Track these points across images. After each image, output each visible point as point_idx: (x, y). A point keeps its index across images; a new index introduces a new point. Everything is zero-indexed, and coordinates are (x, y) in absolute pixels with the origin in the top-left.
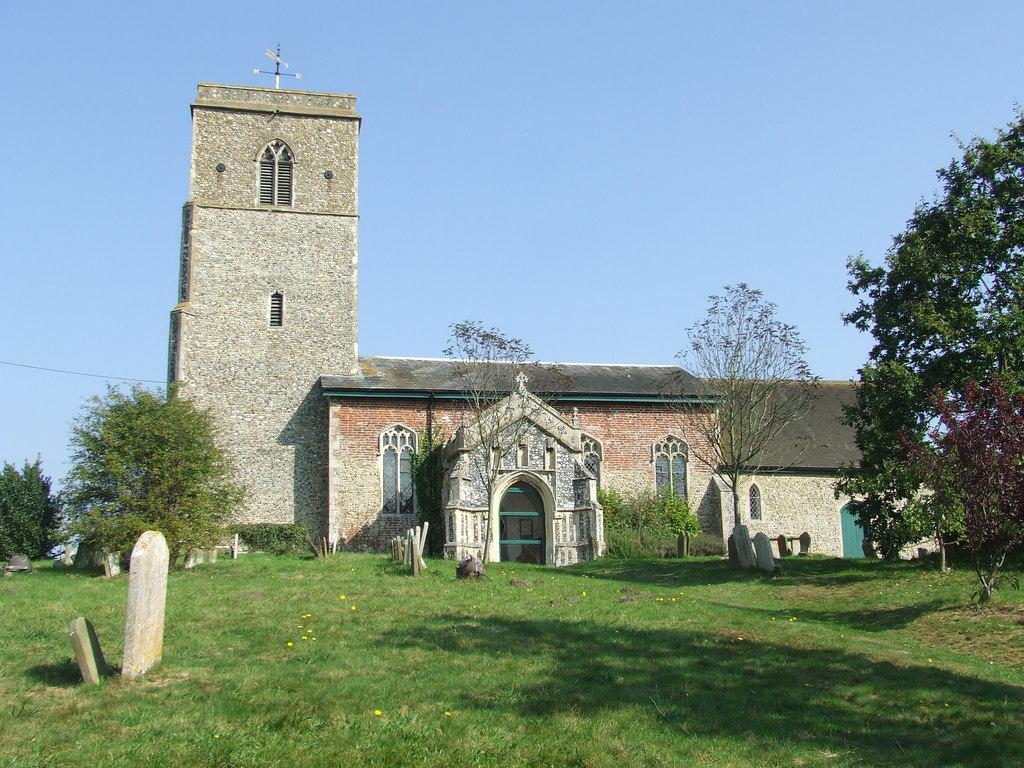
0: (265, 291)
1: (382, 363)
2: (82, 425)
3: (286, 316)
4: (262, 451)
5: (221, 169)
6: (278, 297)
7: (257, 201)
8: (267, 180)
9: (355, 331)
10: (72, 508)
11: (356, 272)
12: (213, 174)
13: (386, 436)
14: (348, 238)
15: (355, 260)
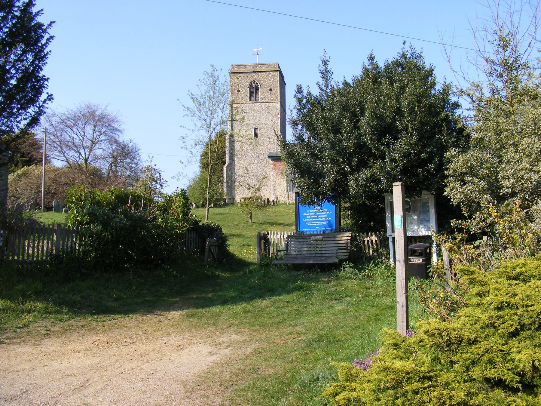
5: (239, 91)
12: (236, 92)
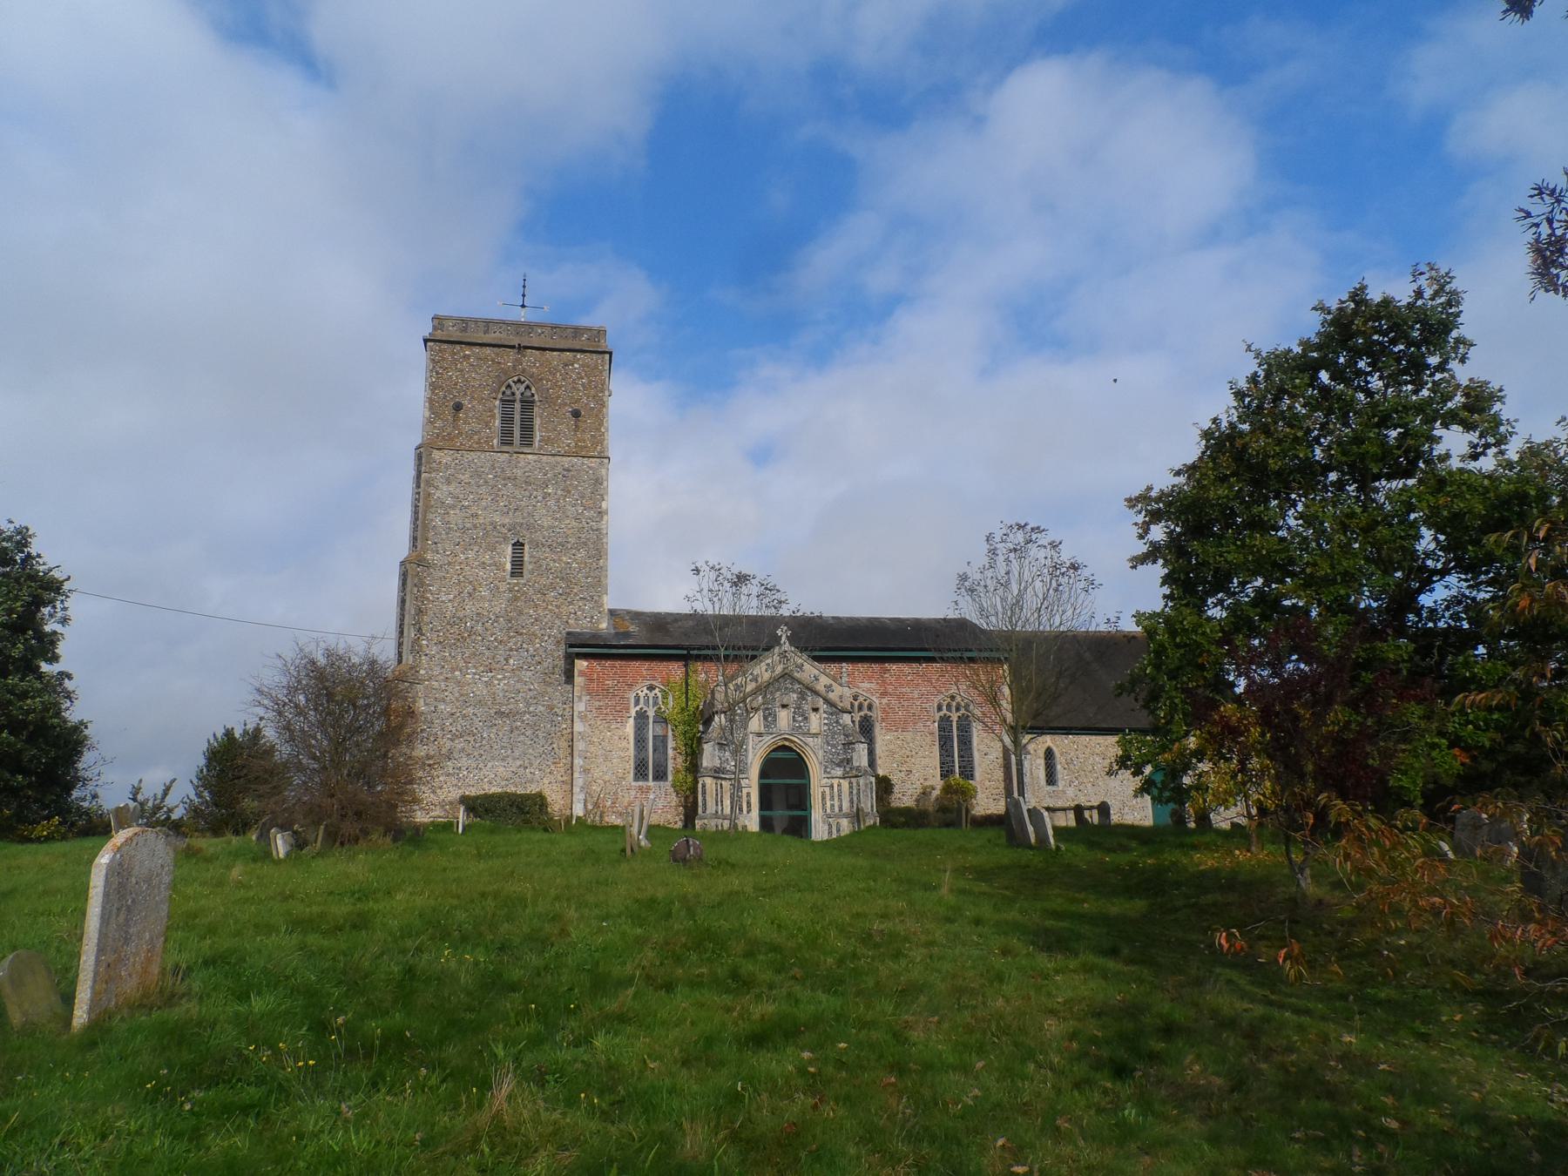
3: (528, 567)
4: (500, 714)
5: (458, 407)
6: (518, 545)
8: (507, 419)
12: (448, 413)
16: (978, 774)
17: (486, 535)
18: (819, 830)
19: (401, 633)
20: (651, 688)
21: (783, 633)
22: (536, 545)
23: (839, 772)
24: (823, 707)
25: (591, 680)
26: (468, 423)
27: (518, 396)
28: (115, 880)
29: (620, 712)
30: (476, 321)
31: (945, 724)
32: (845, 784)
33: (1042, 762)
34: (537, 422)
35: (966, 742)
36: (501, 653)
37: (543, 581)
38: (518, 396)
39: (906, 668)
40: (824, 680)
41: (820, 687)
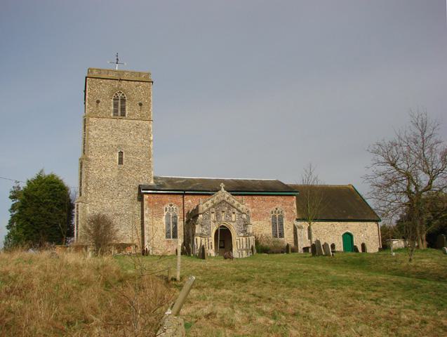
0: (116, 150)
1: (162, 179)
2: (30, 179)
3: (124, 161)
5: (98, 102)
6: (121, 153)
7: (112, 115)
8: (116, 105)
9: (152, 166)
10: (253, 243)
11: (152, 143)
12: (95, 103)
13: (166, 209)
14: (149, 129)
15: (152, 138)
16: (285, 235)
17: (109, 149)
18: (235, 253)
19: (81, 185)
20: (171, 205)
21: (222, 185)
22: (127, 153)
23: (242, 235)
24: (236, 212)
25: (150, 202)
26: (102, 107)
27: (120, 98)
28: (186, 237)
29: (160, 217)
30: (103, 70)
31: (274, 217)
32: (244, 239)
33: (307, 231)
34: (127, 108)
35: (282, 224)
36: (116, 192)
37: (130, 166)
38: (120, 98)
39: (260, 198)
40: (236, 203)
41: (235, 205)
